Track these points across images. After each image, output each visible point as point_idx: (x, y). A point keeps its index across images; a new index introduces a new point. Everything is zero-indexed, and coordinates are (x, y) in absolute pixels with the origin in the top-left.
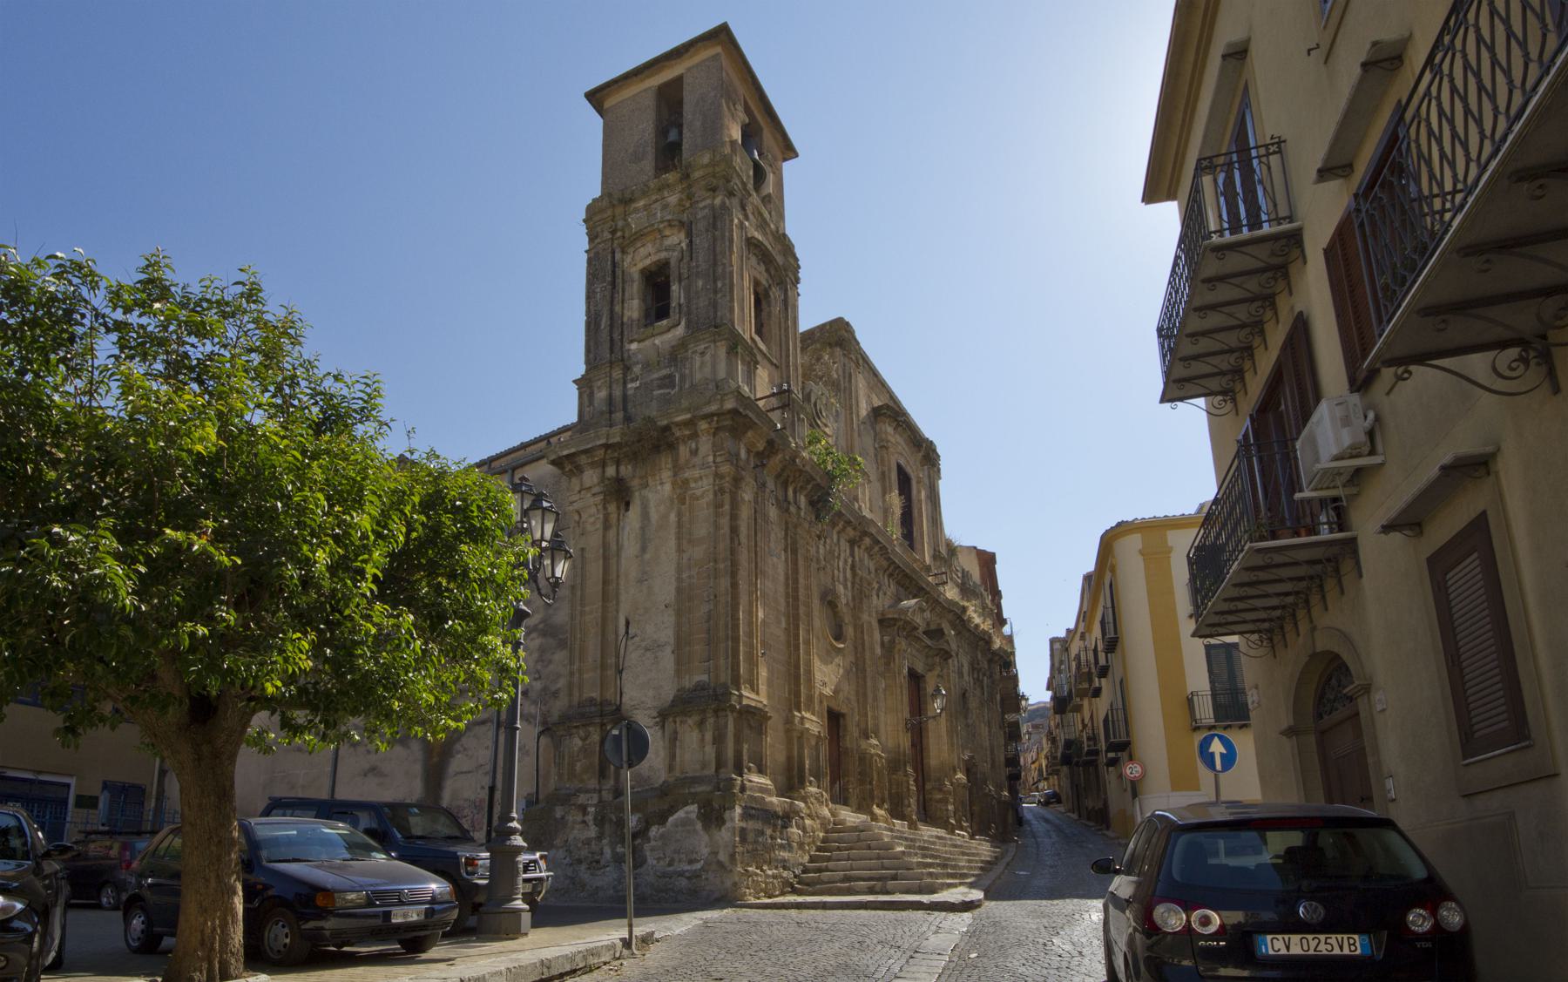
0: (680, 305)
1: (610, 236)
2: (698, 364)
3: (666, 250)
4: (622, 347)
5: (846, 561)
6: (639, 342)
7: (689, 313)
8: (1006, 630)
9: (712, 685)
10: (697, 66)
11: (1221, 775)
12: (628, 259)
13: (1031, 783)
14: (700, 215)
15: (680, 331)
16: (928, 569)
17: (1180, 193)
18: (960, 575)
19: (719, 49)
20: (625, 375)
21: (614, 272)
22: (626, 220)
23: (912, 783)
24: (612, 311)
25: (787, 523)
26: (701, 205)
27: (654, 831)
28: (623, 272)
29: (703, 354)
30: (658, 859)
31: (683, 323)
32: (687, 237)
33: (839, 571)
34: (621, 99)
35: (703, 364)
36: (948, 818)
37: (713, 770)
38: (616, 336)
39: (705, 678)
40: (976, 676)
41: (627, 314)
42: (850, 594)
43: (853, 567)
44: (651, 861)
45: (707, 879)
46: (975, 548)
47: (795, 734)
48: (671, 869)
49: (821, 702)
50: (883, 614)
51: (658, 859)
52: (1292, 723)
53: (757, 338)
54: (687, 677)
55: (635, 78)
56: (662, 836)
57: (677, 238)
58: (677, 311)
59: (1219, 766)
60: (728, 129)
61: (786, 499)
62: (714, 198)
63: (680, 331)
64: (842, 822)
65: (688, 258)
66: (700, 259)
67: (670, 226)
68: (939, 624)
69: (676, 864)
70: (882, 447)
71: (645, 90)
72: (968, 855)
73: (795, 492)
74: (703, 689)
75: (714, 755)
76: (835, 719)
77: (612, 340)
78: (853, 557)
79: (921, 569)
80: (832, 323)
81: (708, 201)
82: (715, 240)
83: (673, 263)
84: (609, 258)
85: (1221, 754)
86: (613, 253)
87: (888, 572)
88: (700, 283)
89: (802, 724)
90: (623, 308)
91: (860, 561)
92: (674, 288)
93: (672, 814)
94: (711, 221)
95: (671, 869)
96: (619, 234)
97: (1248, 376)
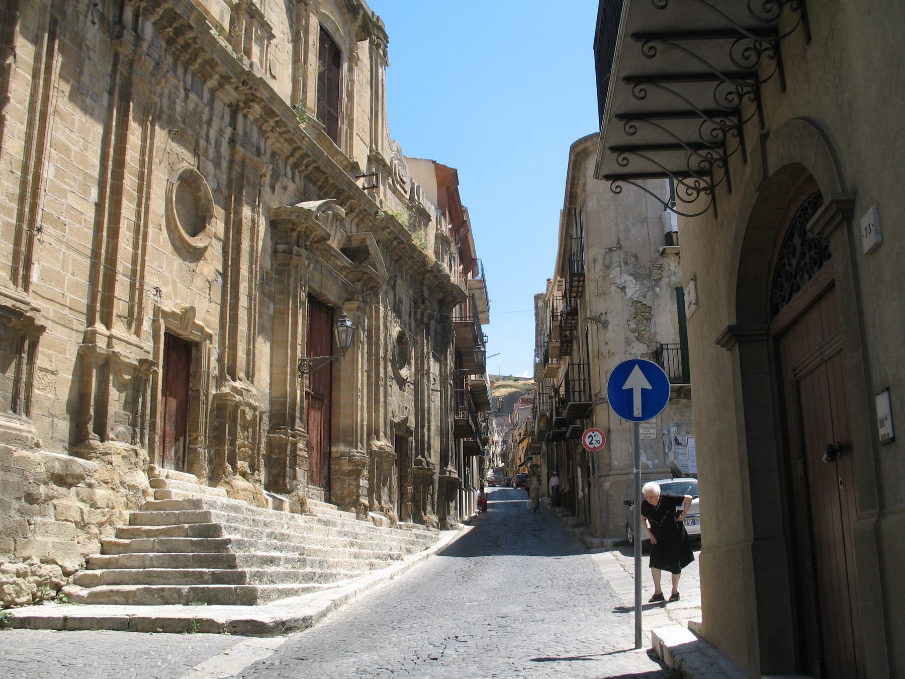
5: (221, 132)
11: (643, 425)
13: (518, 464)
18: (408, 188)
25: (116, 56)
33: (208, 140)
36: (358, 497)
40: (419, 317)
42: (224, 178)
43: (232, 141)
46: (434, 162)
49: (155, 321)
50: (276, 215)
52: (734, 322)
59: (637, 411)
61: (119, 21)
68: (363, 241)
73: (136, 16)
78: (235, 128)
79: (345, 168)
85: (644, 391)
87: (291, 161)
91: (245, 134)
97: (769, 90)
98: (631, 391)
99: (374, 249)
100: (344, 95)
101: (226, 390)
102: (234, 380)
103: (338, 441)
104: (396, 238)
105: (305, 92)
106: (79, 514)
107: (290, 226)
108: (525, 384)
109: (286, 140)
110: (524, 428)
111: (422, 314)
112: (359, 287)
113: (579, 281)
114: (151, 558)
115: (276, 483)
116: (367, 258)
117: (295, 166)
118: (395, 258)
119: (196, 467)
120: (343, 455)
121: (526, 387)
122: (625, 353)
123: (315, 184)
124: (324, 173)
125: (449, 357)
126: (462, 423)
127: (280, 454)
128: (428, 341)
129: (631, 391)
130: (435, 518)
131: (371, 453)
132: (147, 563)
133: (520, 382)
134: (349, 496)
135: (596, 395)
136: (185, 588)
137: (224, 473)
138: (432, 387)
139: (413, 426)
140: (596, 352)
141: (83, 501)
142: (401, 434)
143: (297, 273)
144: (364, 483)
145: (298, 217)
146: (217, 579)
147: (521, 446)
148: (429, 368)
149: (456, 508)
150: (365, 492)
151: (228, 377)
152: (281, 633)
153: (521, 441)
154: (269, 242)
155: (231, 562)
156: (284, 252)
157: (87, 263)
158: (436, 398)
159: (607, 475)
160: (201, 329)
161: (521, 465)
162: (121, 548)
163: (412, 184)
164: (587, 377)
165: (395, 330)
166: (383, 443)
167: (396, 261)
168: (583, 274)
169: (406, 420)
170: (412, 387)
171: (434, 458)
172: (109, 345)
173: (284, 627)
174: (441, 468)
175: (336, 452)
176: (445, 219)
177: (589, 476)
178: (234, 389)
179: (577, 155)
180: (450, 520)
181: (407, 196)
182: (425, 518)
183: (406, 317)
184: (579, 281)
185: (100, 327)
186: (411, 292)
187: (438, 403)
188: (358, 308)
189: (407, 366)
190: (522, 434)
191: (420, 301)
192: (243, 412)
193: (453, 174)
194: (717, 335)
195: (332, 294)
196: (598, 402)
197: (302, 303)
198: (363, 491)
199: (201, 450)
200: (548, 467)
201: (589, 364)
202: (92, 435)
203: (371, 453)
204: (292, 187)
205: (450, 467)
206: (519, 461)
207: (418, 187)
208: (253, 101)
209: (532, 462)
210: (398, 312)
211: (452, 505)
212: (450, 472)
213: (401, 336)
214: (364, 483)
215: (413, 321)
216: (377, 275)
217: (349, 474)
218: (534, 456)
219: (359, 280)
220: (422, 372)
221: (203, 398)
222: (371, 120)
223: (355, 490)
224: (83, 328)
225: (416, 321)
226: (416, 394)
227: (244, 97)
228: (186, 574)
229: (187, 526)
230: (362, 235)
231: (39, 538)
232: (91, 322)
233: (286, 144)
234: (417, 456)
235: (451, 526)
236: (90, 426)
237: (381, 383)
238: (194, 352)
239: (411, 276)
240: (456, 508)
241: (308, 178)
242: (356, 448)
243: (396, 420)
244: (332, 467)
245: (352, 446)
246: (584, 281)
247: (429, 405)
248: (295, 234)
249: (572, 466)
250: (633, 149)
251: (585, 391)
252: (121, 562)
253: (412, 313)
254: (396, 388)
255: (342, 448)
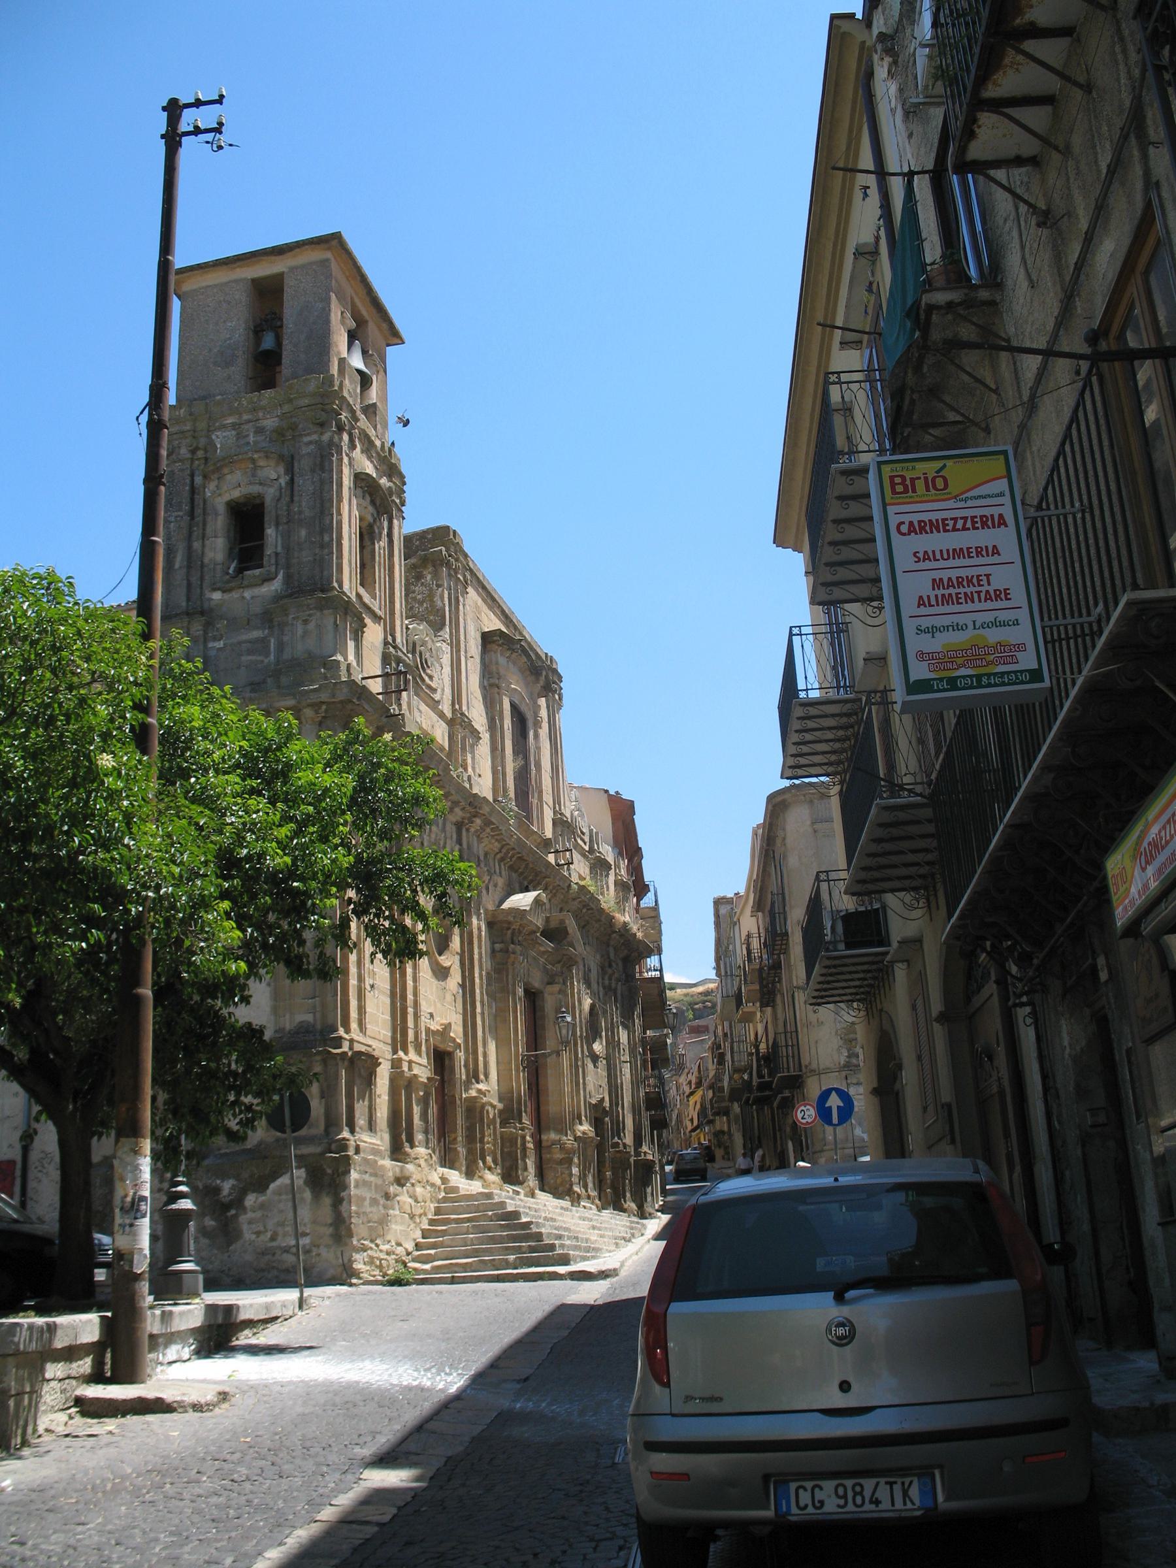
0: (277, 554)
1: (189, 456)
2: (300, 632)
3: (261, 484)
4: (202, 594)
6: (224, 592)
7: (288, 566)
8: (648, 901)
9: (319, 1027)
10: (303, 267)
11: (839, 1129)
12: (212, 486)
13: (690, 1128)
14: (305, 450)
15: (276, 585)
16: (546, 844)
17: (804, 550)
18: (587, 839)
19: (328, 255)
20: (205, 632)
21: (192, 500)
22: (208, 437)
23: (528, 1138)
24: (189, 547)
26: (306, 439)
27: (250, 1200)
28: (205, 501)
29: (306, 622)
30: (258, 1233)
31: (280, 576)
32: (286, 473)
34: (204, 284)
35: (306, 633)
36: (571, 1185)
37: (322, 1127)
38: (195, 580)
39: (309, 1018)
40: (607, 982)
41: (209, 555)
44: (248, 1235)
45: (319, 1255)
46: (606, 791)
47: (403, 1083)
48: (274, 1244)
50: (494, 916)
51: (258, 1233)
53: (362, 591)
54: (288, 1016)
55: (225, 267)
56: (262, 1206)
57: (273, 471)
58: (273, 561)
59: (835, 1120)
60: (337, 346)
62: (322, 434)
63: (276, 585)
64: (455, 1189)
65: (287, 499)
66: (304, 504)
67: (267, 457)
68: (562, 922)
69: (279, 1238)
70: (491, 685)
71: (236, 281)
72: (599, 1229)
74: (307, 1032)
75: (322, 1111)
76: (441, 1059)
77: (189, 585)
78: (461, 844)
80: (438, 528)
81: (315, 437)
82: (322, 482)
83: (268, 501)
84: (188, 481)
85: (838, 1107)
86: (192, 476)
87: (499, 856)
88: (303, 533)
89: (410, 1069)
90: (203, 546)
92: (270, 531)
93: (274, 1179)
94: (318, 461)
95: (274, 1244)
96: (200, 454)
98: (830, 1108)
99: (572, 925)
100: (533, 767)
101: (473, 1093)
102: (478, 1083)
103: (548, 1129)
104: (584, 906)
105: (504, 781)
106: (409, 1208)
107: (505, 925)
108: (686, 995)
109: (497, 840)
110: (696, 1073)
111: (610, 979)
112: (559, 969)
113: (782, 940)
114: (472, 1239)
115: (510, 1175)
116: (565, 937)
117: (502, 859)
118: (583, 924)
119: (457, 1164)
120: (554, 1143)
121: (688, 999)
122: (835, 1022)
123: (516, 871)
124: (526, 860)
125: (637, 1021)
126: (652, 1096)
127: (511, 1146)
128: (617, 1009)
129: (830, 1108)
130: (633, 1206)
131: (576, 1139)
132: (469, 1243)
133: (678, 991)
134: (562, 1184)
135: (806, 1066)
136: (512, 1257)
137: (477, 1168)
138: (622, 1059)
139: (608, 1105)
140: (804, 1021)
141: (411, 1197)
142: (598, 1115)
143: (514, 969)
144: (575, 1170)
145: (514, 917)
146: (532, 1249)
147: (692, 1100)
148: (619, 1039)
149: (652, 1194)
150: (577, 1180)
151: (473, 1080)
152: (602, 1279)
153: (692, 1094)
154: (488, 943)
155: (539, 1236)
156: (501, 950)
157: (388, 1001)
158: (627, 1070)
159: (822, 1151)
160: (454, 1040)
161: (693, 1130)
162: (440, 1234)
163: (591, 831)
164: (795, 1042)
165: (587, 1002)
166: (585, 1128)
167: (583, 927)
168: (786, 934)
169: (603, 1099)
170: (604, 1062)
171: (629, 1139)
172: (410, 1069)
173: (603, 1275)
174: (636, 1150)
175: (547, 1141)
176: (623, 860)
177: (802, 1150)
178: (479, 1091)
179: (774, 806)
180: (648, 1209)
181: (587, 848)
182: (626, 1206)
183: (594, 986)
184: (782, 940)
185: (401, 1053)
186: (598, 957)
187: (628, 1076)
188: (560, 992)
189: (598, 1040)
190: (694, 1081)
191: (607, 964)
192: (488, 1111)
193: (630, 807)
194: (870, 1089)
195: (536, 983)
196: (809, 1074)
197: (520, 999)
198: (575, 1179)
199: (460, 1149)
200: (744, 1136)
201: (797, 1031)
202: (406, 1144)
203: (576, 1139)
204: (501, 882)
205: (645, 1148)
206: (689, 1124)
207: (597, 833)
208: (475, 816)
209: (714, 1127)
210: (588, 984)
211: (649, 1190)
212: (645, 1153)
213: (592, 1007)
214: (575, 1170)
215: (601, 989)
216: (576, 955)
217: (561, 1162)
218: (717, 1118)
219: (559, 962)
220: (613, 1044)
221: (458, 1102)
222: (552, 778)
223: (568, 1179)
224: (389, 1057)
225: (604, 988)
226: (609, 1070)
227: (468, 815)
228: (507, 1248)
229: (490, 1213)
230: (562, 915)
231: (393, 1226)
232: (395, 1052)
233: (496, 844)
234: (613, 1138)
235: (650, 1214)
236: (404, 1137)
237: (580, 1063)
238: (447, 1062)
239: (597, 938)
240: (652, 1194)
241: (511, 868)
242: (566, 1136)
243: (593, 1101)
244: (544, 1156)
245: (562, 1134)
246: (787, 940)
247: (621, 1079)
248: (509, 932)
249: (781, 1138)
250: (842, 564)
251: (793, 1057)
252: (446, 1243)
253: (600, 980)
254: (590, 1066)
255: (553, 1136)
